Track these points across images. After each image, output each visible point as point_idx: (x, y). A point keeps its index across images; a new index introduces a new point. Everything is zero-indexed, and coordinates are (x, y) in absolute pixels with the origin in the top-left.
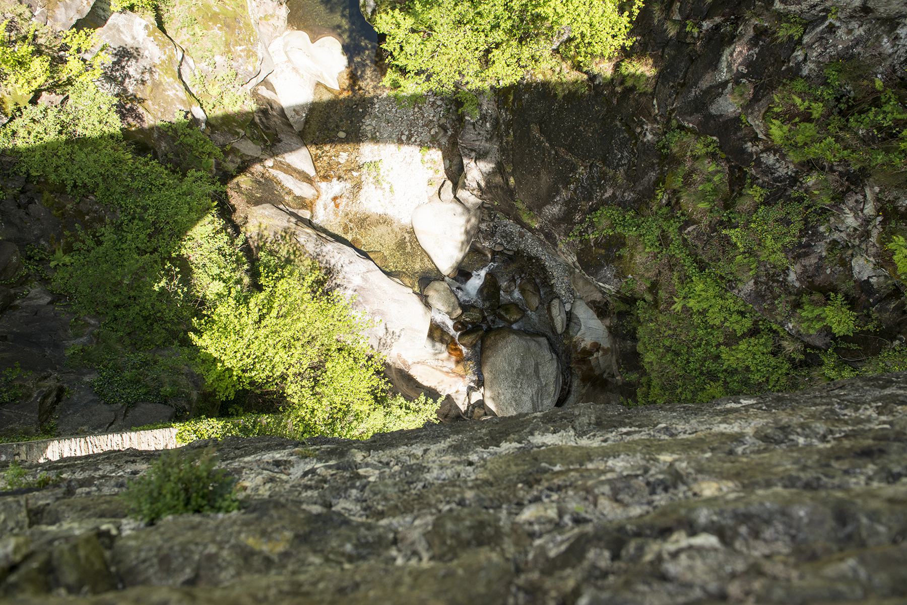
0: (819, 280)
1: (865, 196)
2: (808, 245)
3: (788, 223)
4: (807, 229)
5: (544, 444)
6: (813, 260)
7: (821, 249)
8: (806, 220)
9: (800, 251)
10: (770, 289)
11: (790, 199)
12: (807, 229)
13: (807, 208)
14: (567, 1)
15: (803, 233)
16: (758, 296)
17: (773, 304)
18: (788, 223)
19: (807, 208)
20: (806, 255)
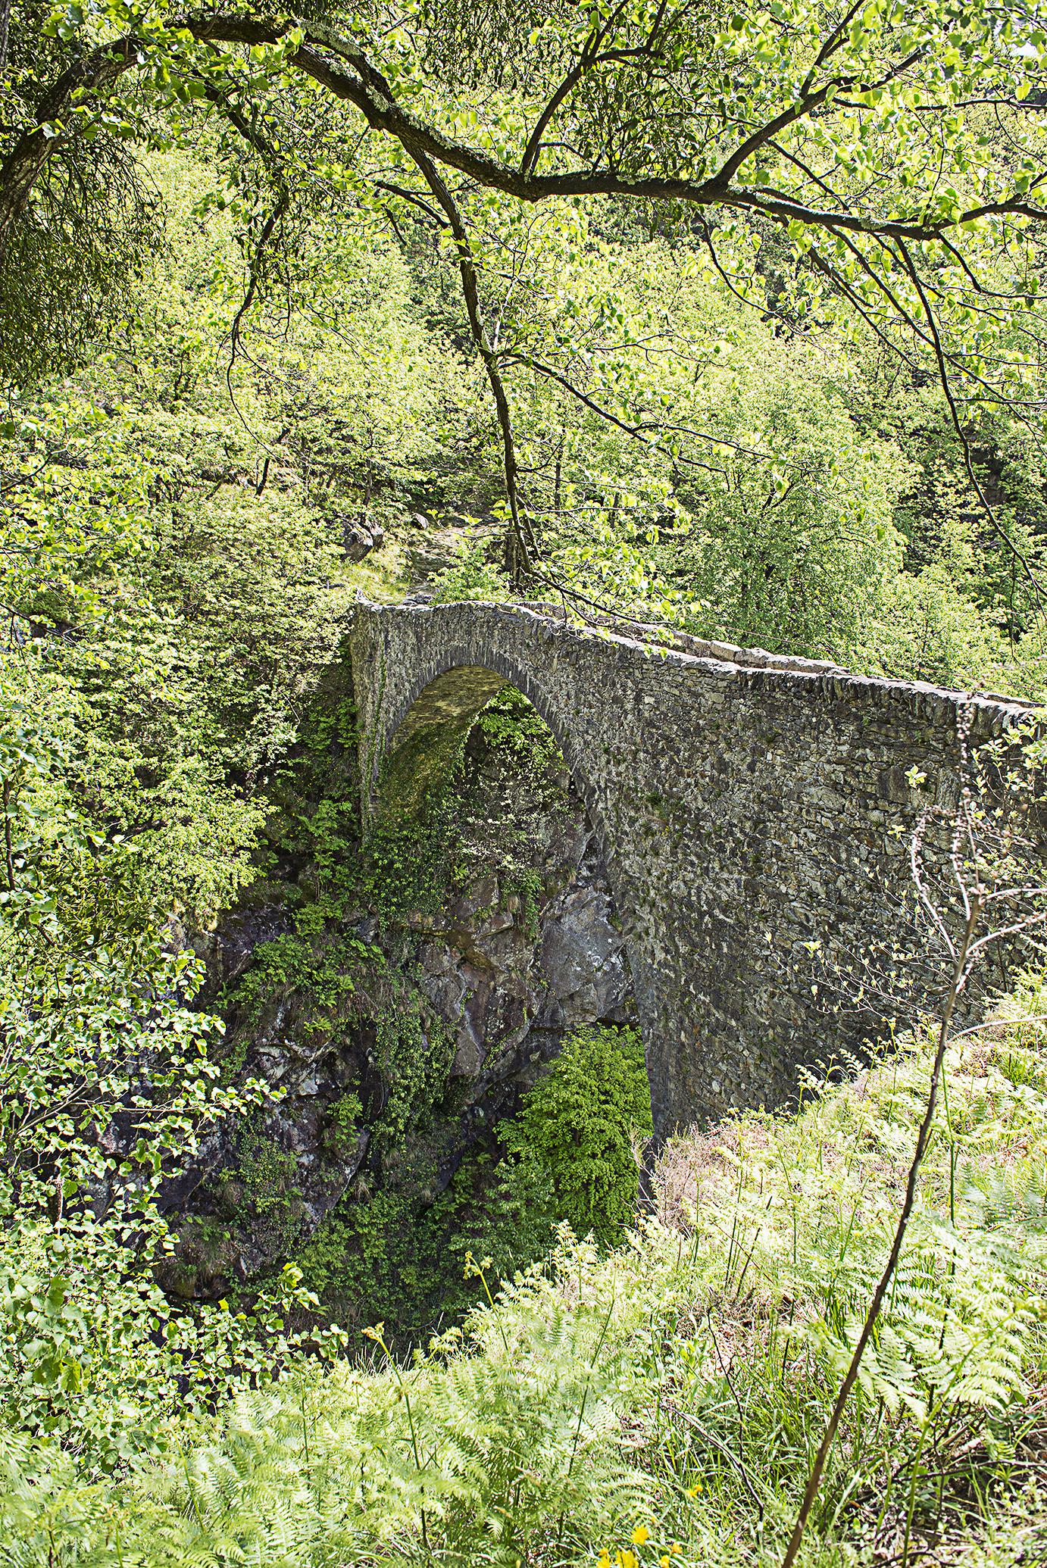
0: (312, 1130)
1: (264, 1054)
2: (281, 1136)
3: (260, 1149)
4: (268, 1135)
5: (970, 1449)
6: (295, 1132)
7: (286, 1124)
8: (259, 1134)
9: (287, 1146)
10: (314, 1185)
11: (238, 1147)
12: (268, 1135)
13: (249, 1131)
14: (309, 2)
15: (270, 1138)
16: (318, 1201)
17: (327, 1185)
18: (260, 1149)
19: (249, 1131)
20: (290, 1139)
